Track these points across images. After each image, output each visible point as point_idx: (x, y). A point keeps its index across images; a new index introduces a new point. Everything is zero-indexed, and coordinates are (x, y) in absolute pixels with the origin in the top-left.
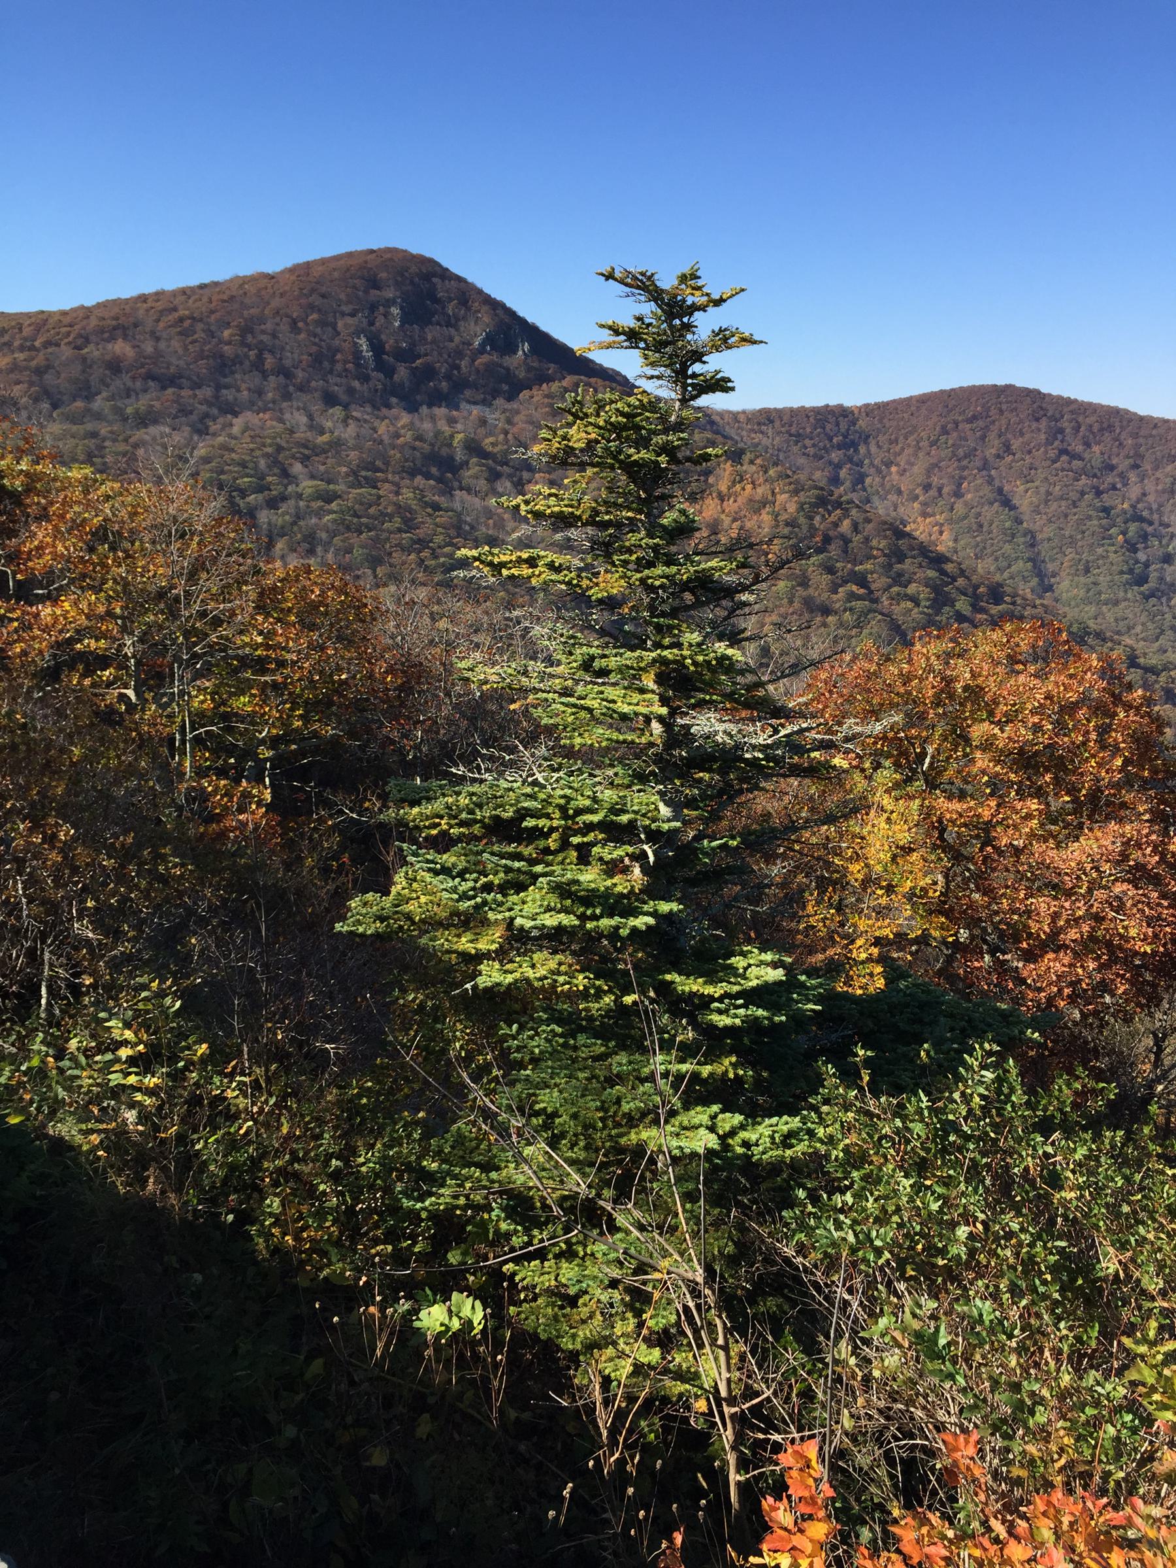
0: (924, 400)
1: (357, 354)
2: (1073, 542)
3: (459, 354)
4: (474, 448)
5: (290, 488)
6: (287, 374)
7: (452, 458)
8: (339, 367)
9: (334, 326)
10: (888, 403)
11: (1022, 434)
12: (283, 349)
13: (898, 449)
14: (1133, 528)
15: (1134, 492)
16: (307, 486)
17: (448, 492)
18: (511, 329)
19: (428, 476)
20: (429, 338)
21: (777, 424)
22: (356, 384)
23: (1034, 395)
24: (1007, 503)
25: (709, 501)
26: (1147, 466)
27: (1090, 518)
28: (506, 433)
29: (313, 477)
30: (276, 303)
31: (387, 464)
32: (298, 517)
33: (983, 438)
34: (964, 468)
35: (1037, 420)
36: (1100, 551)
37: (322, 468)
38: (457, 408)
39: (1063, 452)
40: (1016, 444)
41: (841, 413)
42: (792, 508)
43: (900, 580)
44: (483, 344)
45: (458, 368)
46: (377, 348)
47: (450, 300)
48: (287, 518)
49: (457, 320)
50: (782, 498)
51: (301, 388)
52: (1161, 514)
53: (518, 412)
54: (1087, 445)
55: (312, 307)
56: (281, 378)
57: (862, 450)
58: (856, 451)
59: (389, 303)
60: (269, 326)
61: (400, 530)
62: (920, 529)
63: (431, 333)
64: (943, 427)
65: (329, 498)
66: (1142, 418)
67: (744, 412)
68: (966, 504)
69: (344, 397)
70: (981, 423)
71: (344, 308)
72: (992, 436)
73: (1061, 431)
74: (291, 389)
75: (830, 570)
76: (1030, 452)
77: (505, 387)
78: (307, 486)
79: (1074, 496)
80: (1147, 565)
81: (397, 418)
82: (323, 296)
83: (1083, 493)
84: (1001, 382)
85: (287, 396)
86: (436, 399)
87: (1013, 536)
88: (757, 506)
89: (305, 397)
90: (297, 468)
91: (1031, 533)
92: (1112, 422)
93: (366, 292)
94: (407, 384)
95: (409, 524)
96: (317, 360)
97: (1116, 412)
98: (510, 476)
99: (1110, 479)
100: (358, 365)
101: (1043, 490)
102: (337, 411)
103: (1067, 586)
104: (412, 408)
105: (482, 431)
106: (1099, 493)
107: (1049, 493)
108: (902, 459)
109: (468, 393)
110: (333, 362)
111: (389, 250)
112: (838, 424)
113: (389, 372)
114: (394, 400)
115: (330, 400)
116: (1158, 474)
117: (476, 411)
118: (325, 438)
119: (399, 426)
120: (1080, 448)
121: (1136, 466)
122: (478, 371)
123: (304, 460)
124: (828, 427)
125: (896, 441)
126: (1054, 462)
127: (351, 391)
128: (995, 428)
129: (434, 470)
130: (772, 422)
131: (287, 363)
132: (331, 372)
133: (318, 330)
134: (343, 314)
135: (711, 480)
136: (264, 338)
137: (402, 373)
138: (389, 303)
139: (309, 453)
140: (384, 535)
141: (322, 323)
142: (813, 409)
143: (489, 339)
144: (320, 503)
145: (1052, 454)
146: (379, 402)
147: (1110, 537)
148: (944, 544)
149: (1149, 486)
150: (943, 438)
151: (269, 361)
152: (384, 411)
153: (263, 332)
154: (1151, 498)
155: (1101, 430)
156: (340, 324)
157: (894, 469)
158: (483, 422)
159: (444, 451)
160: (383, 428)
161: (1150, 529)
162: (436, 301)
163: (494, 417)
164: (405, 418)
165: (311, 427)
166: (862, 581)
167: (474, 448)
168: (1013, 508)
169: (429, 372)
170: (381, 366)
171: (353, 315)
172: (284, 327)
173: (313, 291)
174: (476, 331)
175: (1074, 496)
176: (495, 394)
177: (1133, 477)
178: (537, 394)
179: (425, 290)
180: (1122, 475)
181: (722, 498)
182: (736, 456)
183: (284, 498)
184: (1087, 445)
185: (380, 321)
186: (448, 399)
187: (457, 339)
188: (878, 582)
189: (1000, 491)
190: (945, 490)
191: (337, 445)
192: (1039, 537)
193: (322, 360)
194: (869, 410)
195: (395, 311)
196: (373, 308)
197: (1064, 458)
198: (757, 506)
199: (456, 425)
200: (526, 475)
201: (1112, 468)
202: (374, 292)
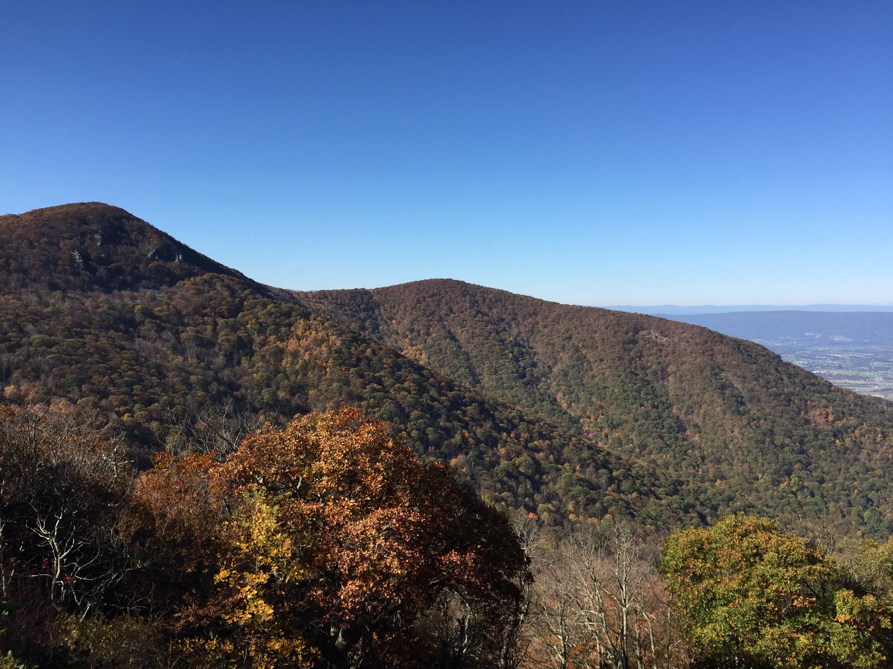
0: (407, 286)
1: (72, 260)
2: (488, 358)
3: (139, 261)
4: (147, 313)
5: (24, 340)
6: (25, 272)
7: (133, 319)
8: (60, 268)
9: (58, 245)
10: (388, 288)
11: (458, 303)
12: (23, 258)
13: (395, 311)
14: (516, 350)
15: (515, 331)
16: (36, 337)
17: (131, 338)
18: (170, 247)
19: (117, 330)
20: (119, 251)
21: (330, 298)
22: (71, 278)
23: (462, 284)
24: (453, 338)
25: (291, 340)
26: (520, 319)
27: (494, 345)
28: (168, 305)
29: (40, 332)
30: (20, 231)
31: (91, 323)
32: (29, 356)
33: (438, 305)
34: (430, 321)
35: (465, 296)
36: (501, 361)
37: (47, 327)
38: (137, 291)
39: (479, 312)
40: (455, 308)
41: (364, 293)
42: (338, 343)
43: (400, 380)
44: (153, 256)
45: (138, 268)
46: (85, 257)
47: (133, 231)
48: (21, 357)
49: (138, 242)
50: (333, 338)
51: (34, 281)
52: (528, 342)
53: (176, 293)
54: (490, 309)
55: (43, 234)
56: (21, 275)
57: (377, 312)
58: (373, 312)
59: (94, 232)
60: (14, 244)
61: (98, 362)
62: (410, 352)
63: (120, 249)
64: (418, 300)
65: (50, 345)
66: (515, 295)
67: (311, 292)
68: (432, 339)
69: (62, 285)
70: (436, 298)
71: (65, 235)
72: (443, 304)
73: (477, 302)
74: (27, 281)
75: (361, 376)
76: (462, 312)
77: (167, 279)
78: (36, 337)
79: (486, 334)
80: (524, 368)
81: (98, 297)
82: (51, 228)
83: (490, 333)
84: (445, 277)
85: (24, 285)
86: (123, 286)
87: (458, 355)
88: (319, 343)
89: (36, 285)
90: (30, 327)
91: (466, 353)
92: (501, 297)
93: (79, 226)
94: (105, 277)
95: (104, 358)
96: (46, 264)
97: (502, 292)
98: (170, 329)
99: (503, 325)
100: (72, 267)
101: (470, 331)
102: (58, 294)
103: (487, 380)
104: (108, 291)
105: (153, 304)
106: (498, 333)
107: (473, 333)
108: (398, 317)
109: (144, 282)
110: (56, 265)
111: (94, 203)
112: (362, 299)
113: (93, 271)
114: (96, 287)
115: (53, 287)
116: (525, 323)
117: (149, 293)
118: (49, 309)
119: (99, 302)
120: (486, 310)
121: (514, 319)
122: (150, 270)
123: (35, 322)
124: (358, 300)
125: (394, 307)
126: (475, 317)
127: (67, 282)
128: (444, 300)
129: (122, 327)
130: (327, 297)
131: (26, 266)
132: (55, 271)
133: (47, 247)
134: (64, 238)
135: (292, 329)
136: (11, 252)
137: (102, 271)
138: (94, 232)
139: (37, 318)
140: (88, 365)
141: (50, 243)
142: (349, 291)
143: (157, 253)
144: (44, 348)
145: (473, 313)
146: (86, 288)
147: (506, 354)
148: (423, 360)
149: (522, 329)
150: (418, 306)
151: (13, 264)
152: (90, 293)
153: (10, 248)
154: (523, 335)
155: (496, 301)
156: (61, 244)
157: (394, 321)
158: (154, 299)
159: (129, 316)
160: (88, 303)
161: (524, 350)
162: (126, 232)
163: (161, 296)
164: (103, 297)
165: (40, 303)
166: (379, 381)
167: (147, 313)
168: (456, 341)
169: (119, 271)
170: (87, 267)
171: (70, 239)
172: (25, 245)
173: (44, 225)
174: (150, 249)
175: (486, 334)
176: (161, 283)
177: (514, 325)
178: (188, 283)
179: (117, 225)
180: (507, 323)
181: (299, 338)
182: (306, 316)
183: (19, 345)
184: (490, 309)
185: (88, 242)
186: (132, 286)
187: (137, 253)
188: (388, 381)
189: (449, 332)
190: (422, 332)
191: (57, 313)
192: (471, 355)
193: (49, 264)
194: (379, 291)
195: (98, 237)
196: (83, 235)
197: (480, 315)
198: (319, 343)
199: (136, 301)
200: (181, 328)
201: (503, 320)
202: (83, 226)
